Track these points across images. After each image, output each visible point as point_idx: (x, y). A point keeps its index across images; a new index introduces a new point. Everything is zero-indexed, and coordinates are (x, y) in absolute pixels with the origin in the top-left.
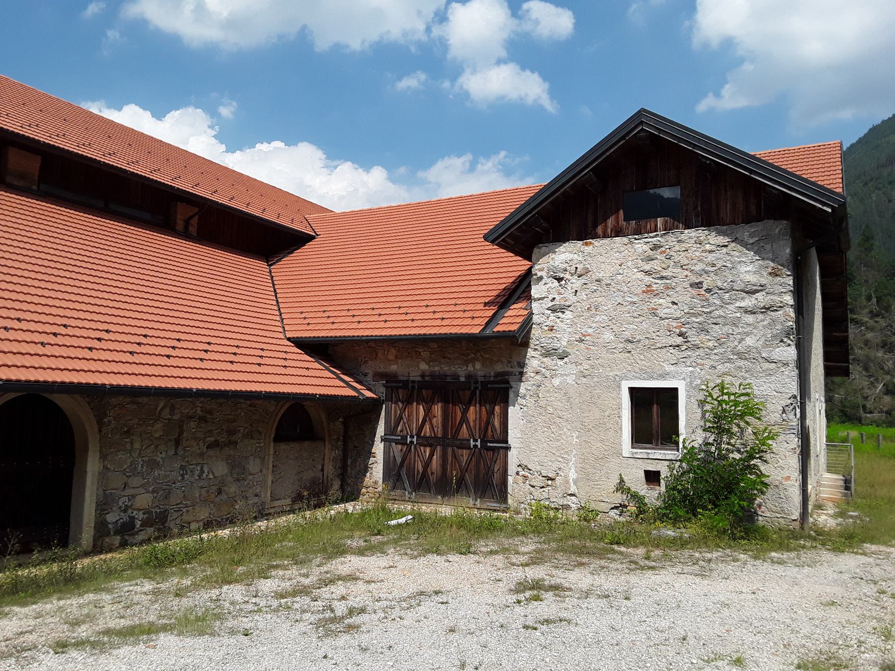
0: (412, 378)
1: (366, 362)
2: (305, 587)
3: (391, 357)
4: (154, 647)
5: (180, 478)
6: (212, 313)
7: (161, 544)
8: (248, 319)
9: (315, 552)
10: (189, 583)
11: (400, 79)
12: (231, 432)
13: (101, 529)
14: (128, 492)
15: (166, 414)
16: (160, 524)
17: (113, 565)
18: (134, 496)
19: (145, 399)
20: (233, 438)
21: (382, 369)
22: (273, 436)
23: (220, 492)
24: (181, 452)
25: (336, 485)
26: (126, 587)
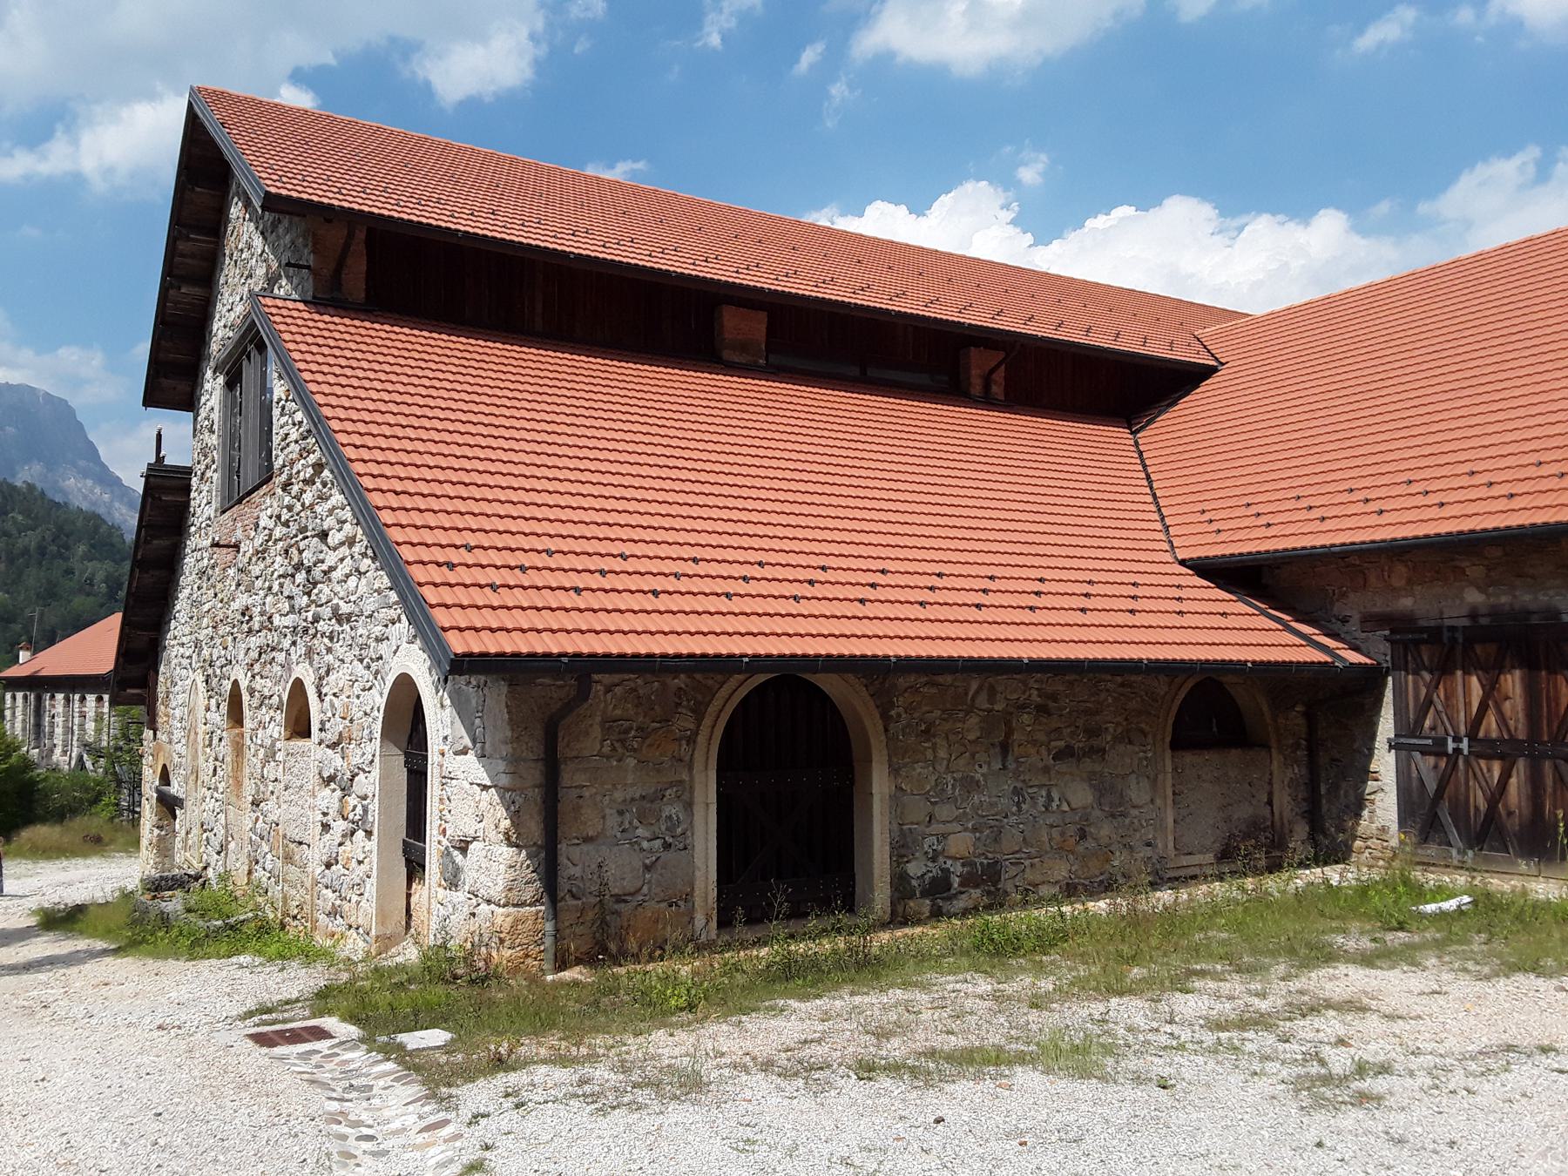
0: (1448, 622)
1: (1344, 595)
2: (1262, 1015)
3: (1397, 582)
4: (1010, 1088)
5: (1014, 809)
6: (1042, 528)
7: (997, 918)
8: (1104, 533)
9: (1273, 954)
10: (1051, 987)
11: (1360, 31)
12: (1093, 732)
13: (901, 887)
14: (936, 828)
15: (982, 702)
16: (989, 883)
17: (925, 945)
18: (945, 836)
19: (949, 679)
20: (1095, 742)
21: (1379, 606)
22: (1168, 739)
23: (1083, 835)
24: (1012, 766)
25: (1302, 830)
26: (950, 983)
